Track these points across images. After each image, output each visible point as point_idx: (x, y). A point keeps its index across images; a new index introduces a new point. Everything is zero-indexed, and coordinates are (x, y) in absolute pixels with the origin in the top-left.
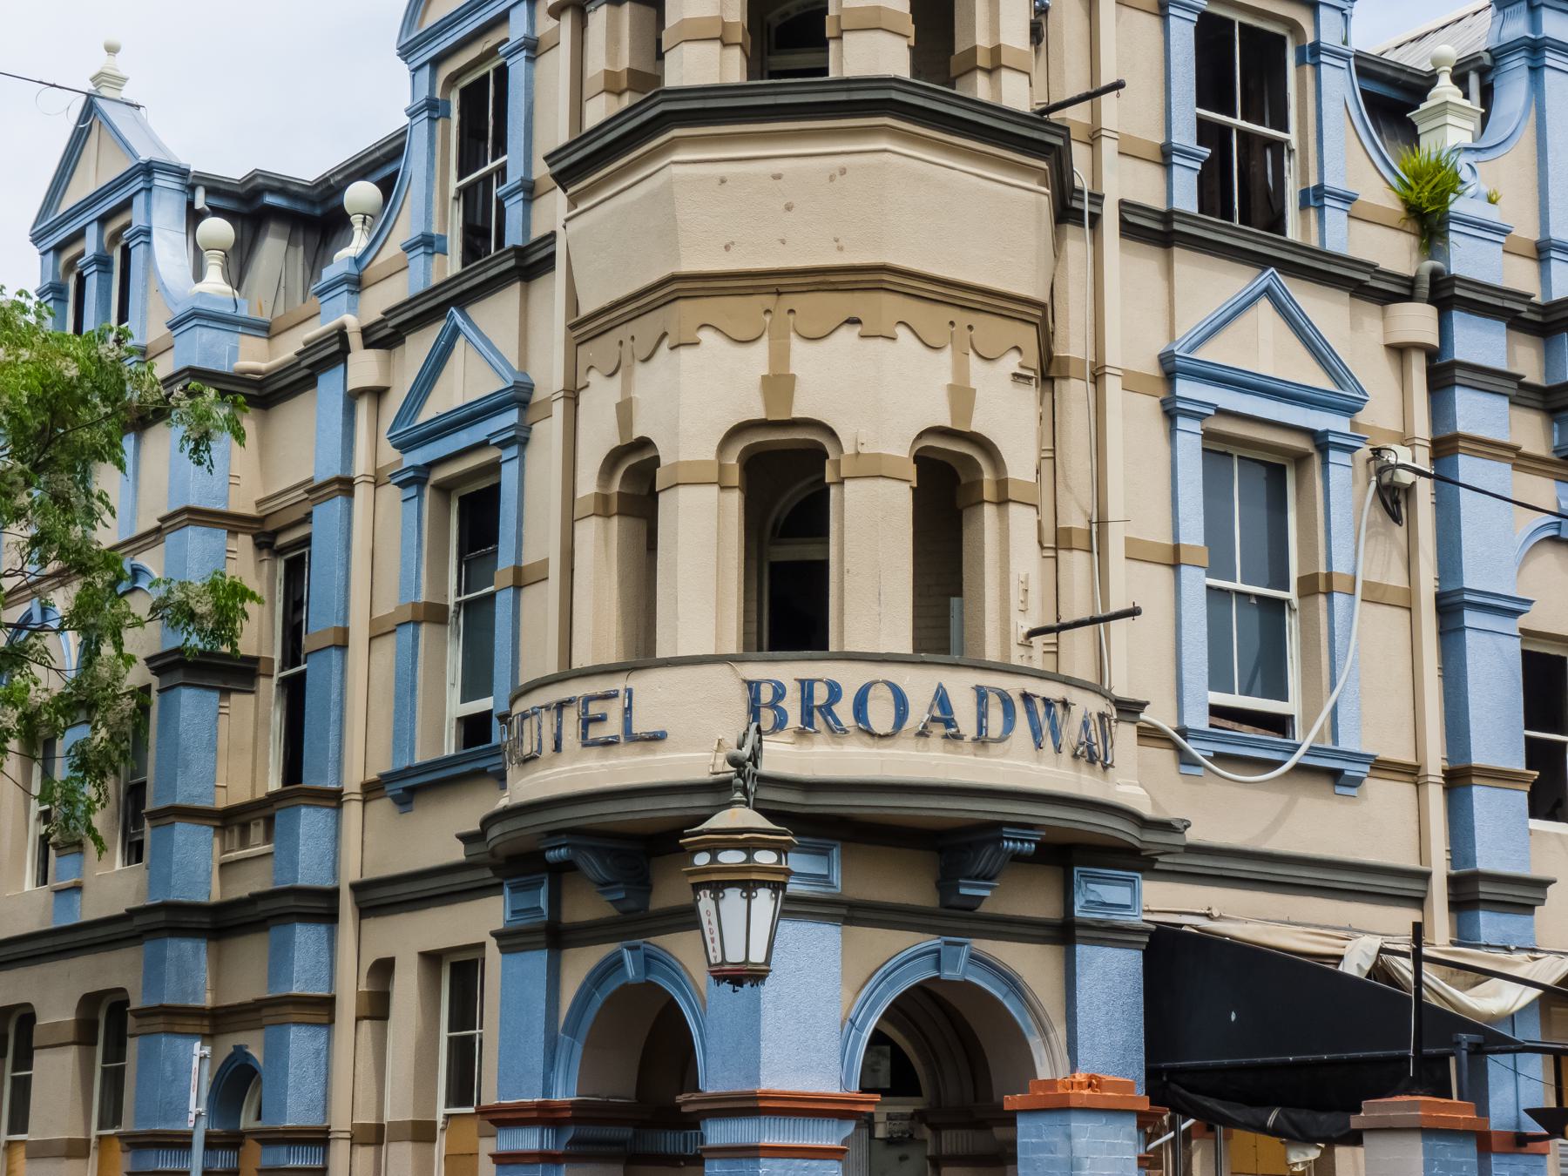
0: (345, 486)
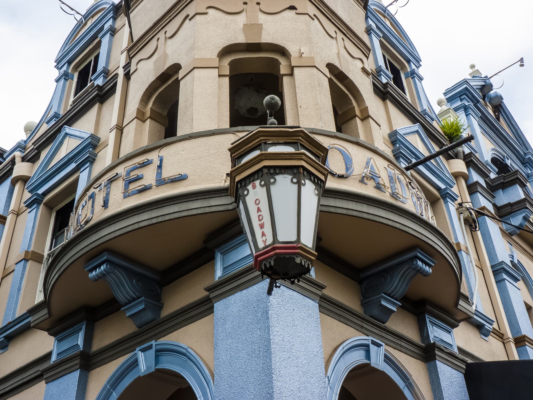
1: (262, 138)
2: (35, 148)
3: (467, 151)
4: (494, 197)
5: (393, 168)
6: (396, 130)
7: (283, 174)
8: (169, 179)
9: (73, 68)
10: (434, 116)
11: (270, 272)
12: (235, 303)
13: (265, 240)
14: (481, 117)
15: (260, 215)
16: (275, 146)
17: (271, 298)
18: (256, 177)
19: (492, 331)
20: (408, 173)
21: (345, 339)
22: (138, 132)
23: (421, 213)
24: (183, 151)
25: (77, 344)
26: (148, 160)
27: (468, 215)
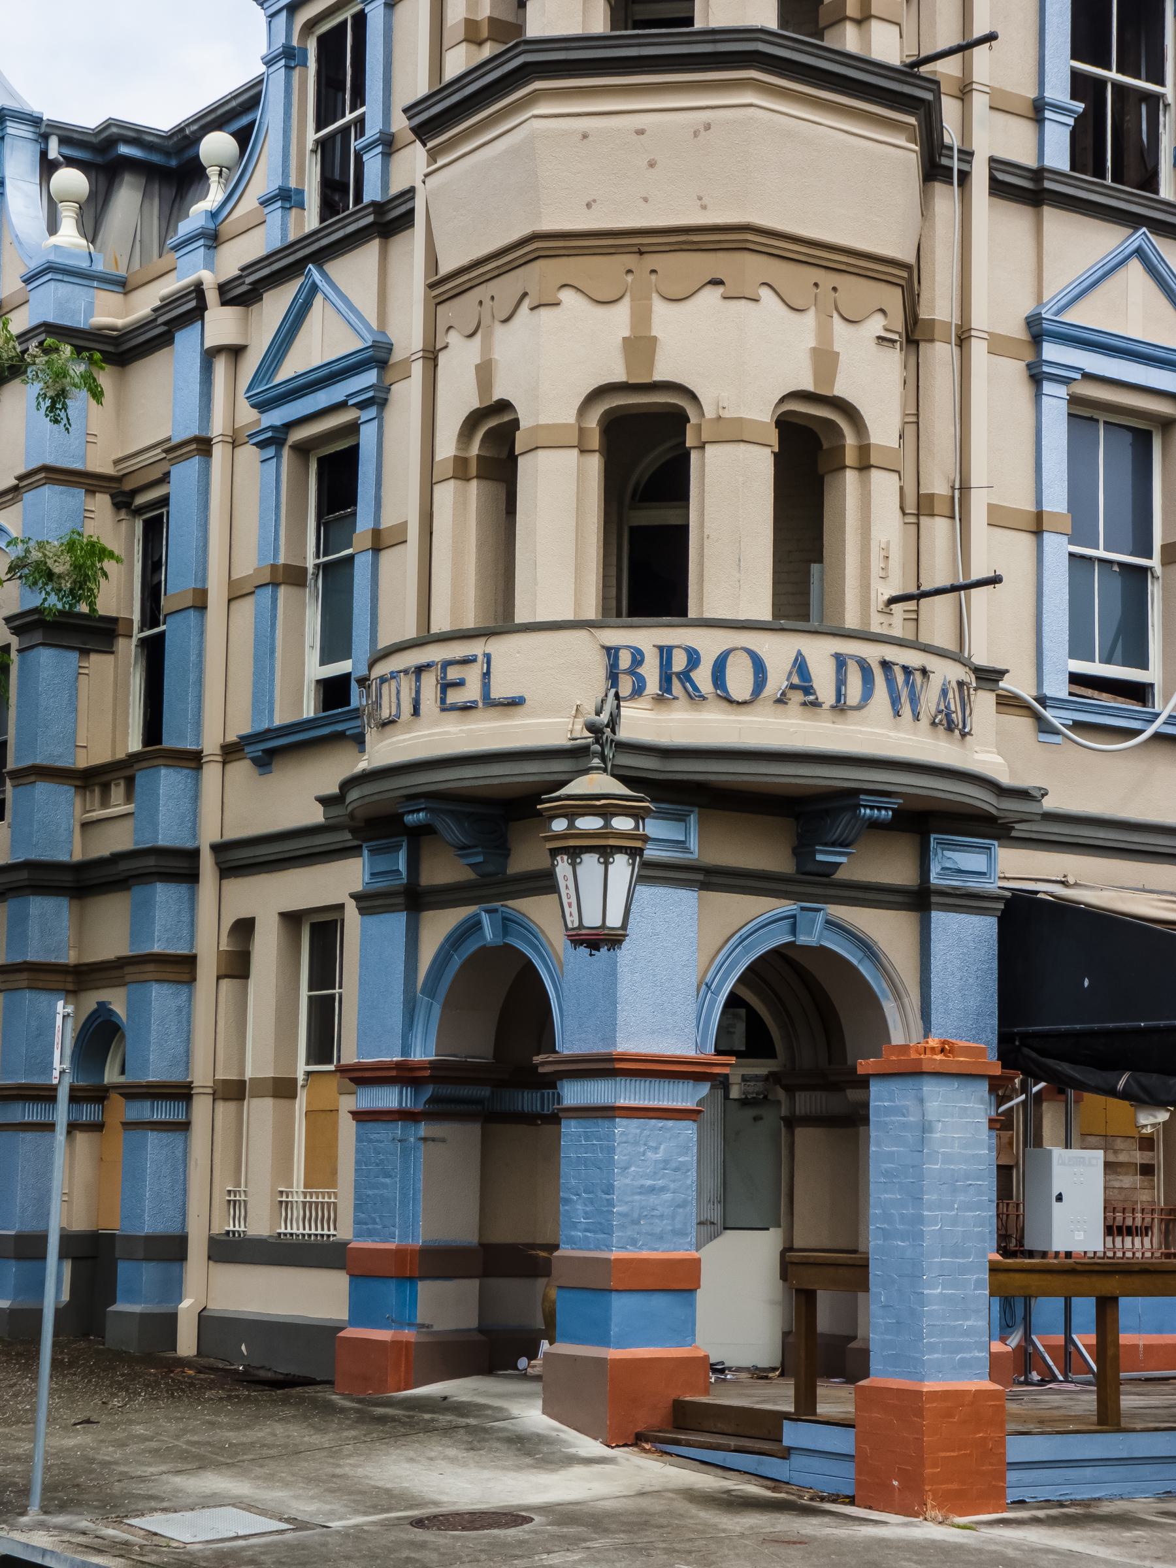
0: (203, 445)
9: (299, 35)
24: (518, 653)
25: (398, 870)
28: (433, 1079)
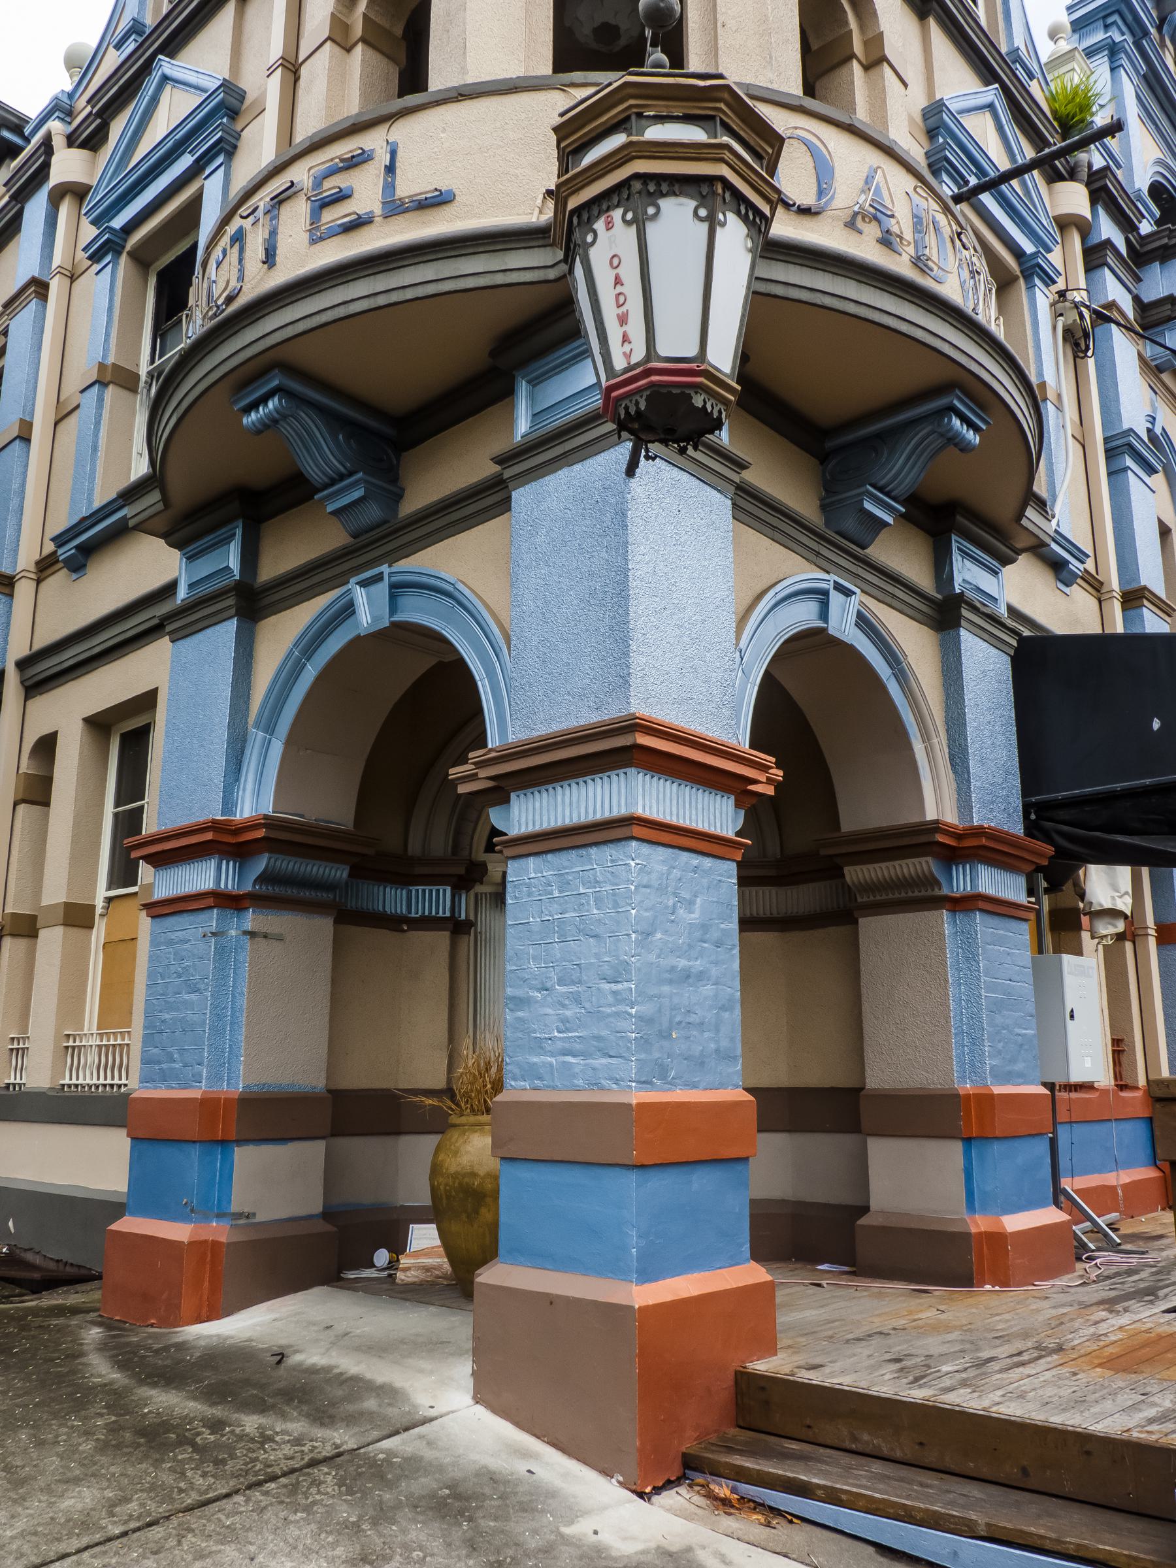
1: (632, 102)
2: (94, 112)
3: (1098, 162)
4: (1138, 280)
5: (925, 195)
6: (942, 99)
7: (676, 195)
8: (413, 201)
10: (1034, 67)
11: (636, 426)
12: (557, 491)
13: (628, 353)
14: (1144, 76)
15: (620, 294)
16: (663, 123)
17: (633, 483)
18: (615, 200)
19: (1080, 574)
20: (956, 209)
21: (781, 577)
22: (337, 77)
23: (974, 309)
24: (444, 131)
25: (228, 567)
26: (364, 151)
27: (1075, 320)
28: (269, 844)
